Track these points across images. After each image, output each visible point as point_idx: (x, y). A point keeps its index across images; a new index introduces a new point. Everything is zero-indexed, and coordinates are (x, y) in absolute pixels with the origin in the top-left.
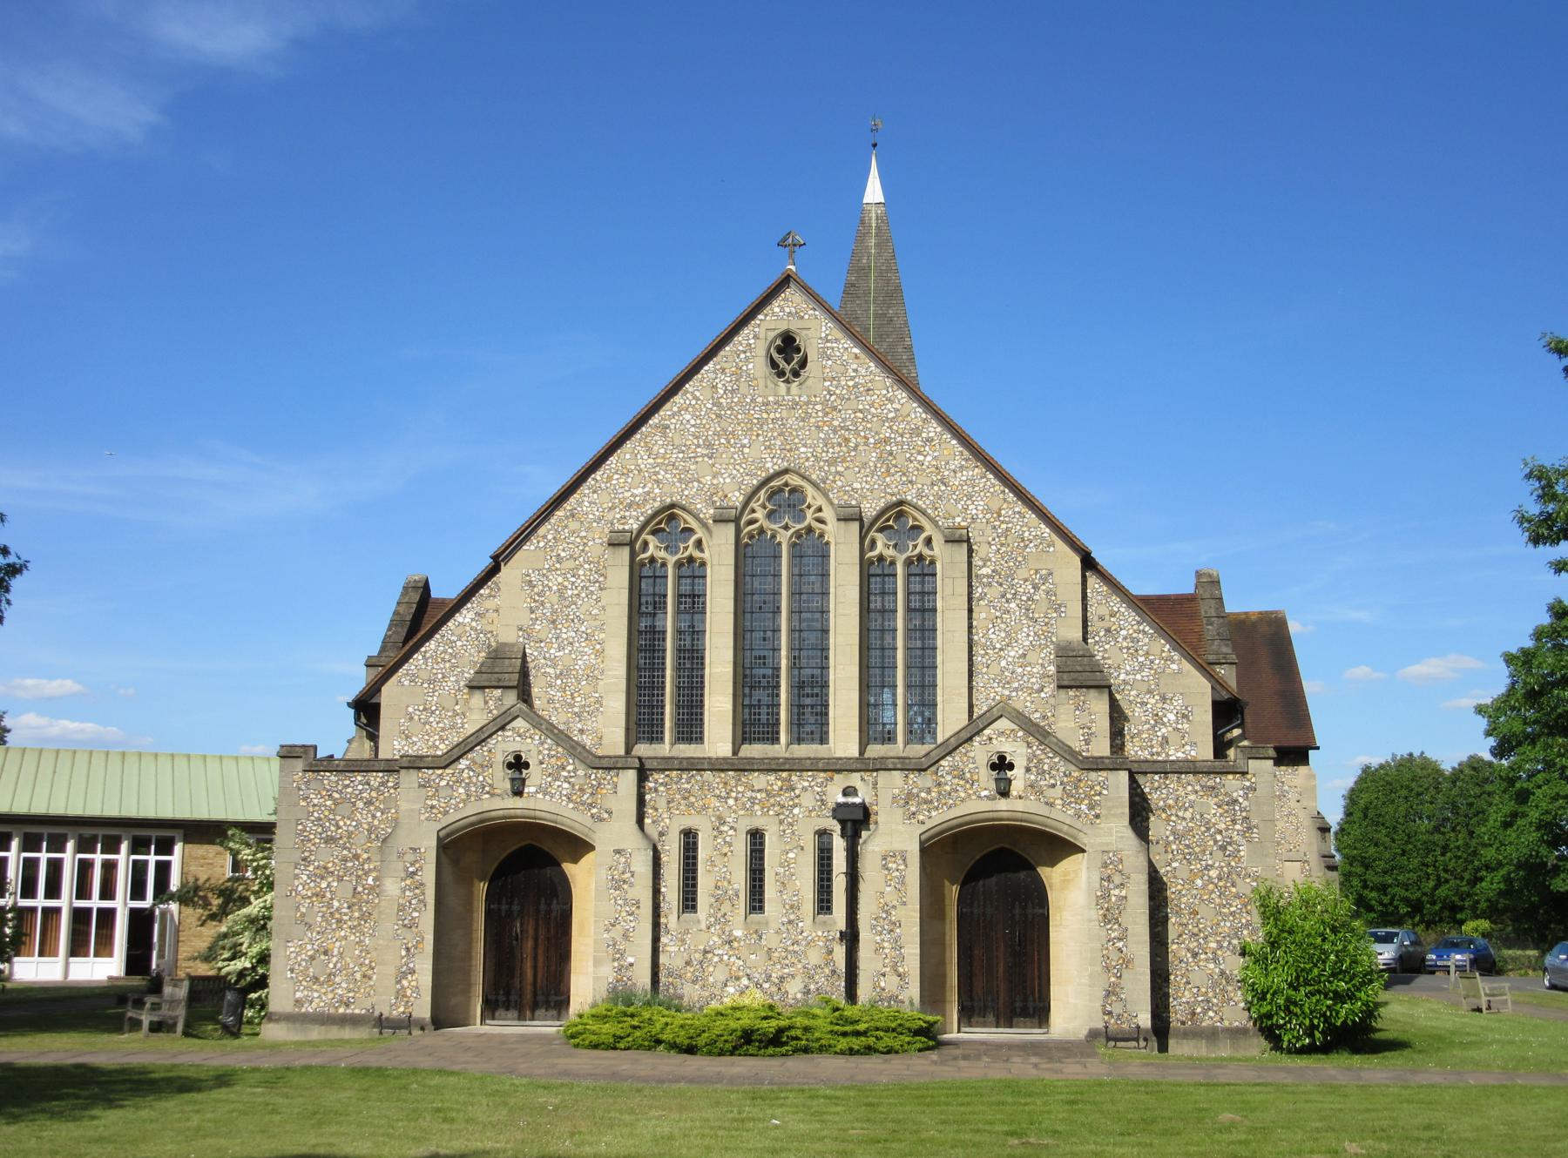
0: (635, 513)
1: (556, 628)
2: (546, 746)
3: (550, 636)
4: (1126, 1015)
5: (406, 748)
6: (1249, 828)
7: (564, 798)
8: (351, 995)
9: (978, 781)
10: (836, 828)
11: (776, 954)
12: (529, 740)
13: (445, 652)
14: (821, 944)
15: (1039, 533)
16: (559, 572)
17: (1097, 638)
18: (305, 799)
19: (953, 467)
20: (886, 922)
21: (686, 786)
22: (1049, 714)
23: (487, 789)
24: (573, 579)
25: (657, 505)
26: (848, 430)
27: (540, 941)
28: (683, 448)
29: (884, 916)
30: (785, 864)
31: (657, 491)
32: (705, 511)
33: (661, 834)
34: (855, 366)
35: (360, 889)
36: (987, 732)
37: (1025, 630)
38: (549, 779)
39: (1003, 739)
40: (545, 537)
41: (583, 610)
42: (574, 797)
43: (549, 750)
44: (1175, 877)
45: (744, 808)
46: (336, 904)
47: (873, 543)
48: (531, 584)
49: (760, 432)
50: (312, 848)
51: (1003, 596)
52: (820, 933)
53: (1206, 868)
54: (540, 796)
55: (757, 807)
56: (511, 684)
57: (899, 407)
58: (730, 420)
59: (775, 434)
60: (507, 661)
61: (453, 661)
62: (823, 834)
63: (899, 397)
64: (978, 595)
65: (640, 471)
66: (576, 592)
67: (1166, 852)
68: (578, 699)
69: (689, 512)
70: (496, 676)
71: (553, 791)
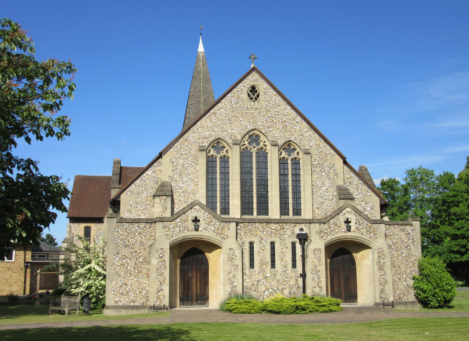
0: (206, 141)
1: (181, 177)
2: (206, 215)
3: (180, 179)
4: (386, 298)
5: (130, 216)
6: (414, 242)
7: (212, 232)
8: (135, 299)
9: (341, 227)
11: (280, 281)
12: (200, 213)
13: (142, 184)
14: (294, 278)
15: (331, 152)
16: (182, 159)
17: (347, 185)
18: (117, 232)
21: (250, 228)
22: (335, 207)
23: (186, 228)
24: (187, 161)
26: (273, 117)
27: (198, 279)
28: (222, 121)
29: (315, 269)
30: (282, 253)
31: (213, 134)
32: (229, 141)
33: (243, 243)
34: (275, 98)
35: (137, 263)
36: (343, 212)
37: (327, 181)
38: (207, 225)
39: (348, 214)
40: (177, 147)
41: (190, 171)
42: (216, 231)
44: (393, 256)
45: (269, 235)
46: (129, 268)
47: (281, 153)
49: (246, 117)
50: (120, 249)
51: (321, 171)
52: (294, 275)
53: (402, 254)
54: (204, 231)
55: (273, 235)
56: (169, 195)
57: (288, 111)
59: (251, 118)
60: (166, 187)
61: (145, 187)
62: (293, 244)
63: (288, 108)
64: (313, 170)
65: (208, 127)
66: (188, 165)
68: (189, 200)
70: (164, 192)
71: (209, 229)
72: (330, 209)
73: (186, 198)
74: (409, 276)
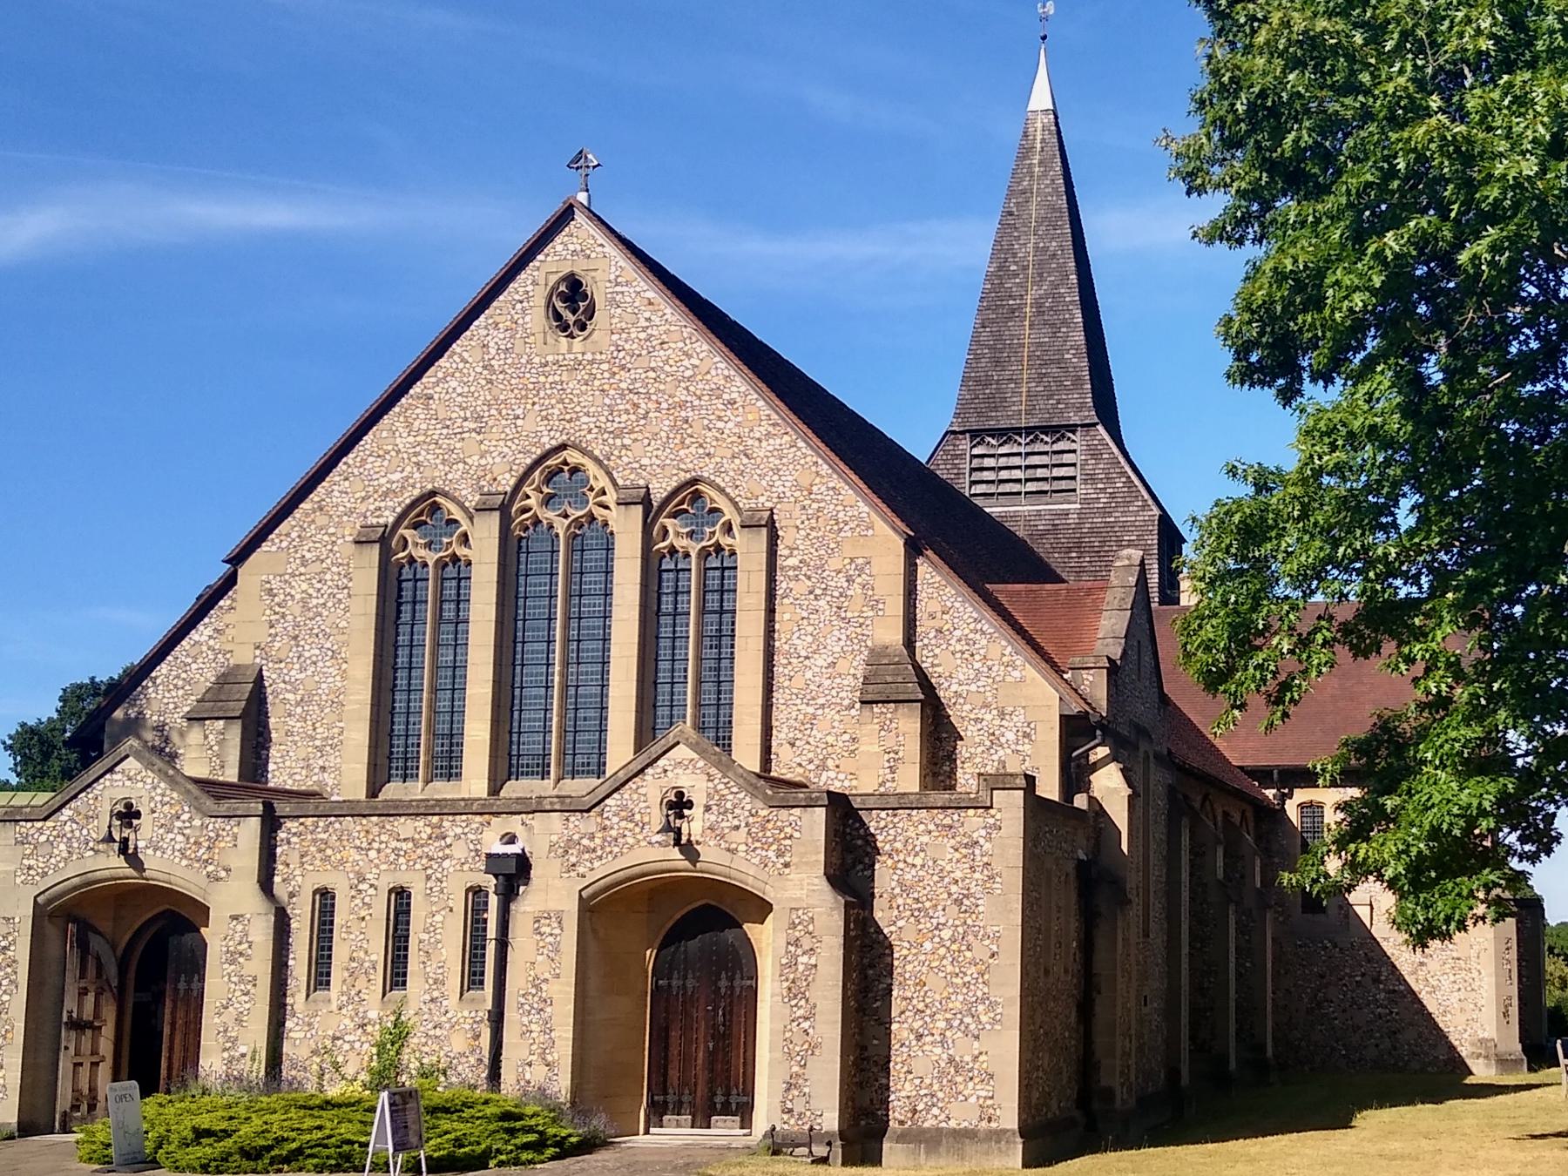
0: (391, 504)
1: (298, 646)
4: (808, 1113)
7: (177, 854)
9: (649, 823)
10: (490, 882)
13: (178, 677)
16: (303, 578)
19: (758, 435)
20: (536, 999)
24: (319, 586)
25: (417, 492)
29: (534, 991)
31: (417, 475)
33: (292, 895)
34: (647, 315)
36: (661, 762)
37: (836, 633)
38: (161, 831)
40: (288, 535)
43: (163, 795)
44: (900, 940)
48: (270, 592)
49: (536, 400)
52: (466, 1013)
55: (402, 860)
58: (501, 386)
59: (553, 401)
61: (187, 687)
62: (477, 892)
65: (398, 452)
66: (321, 601)
67: (891, 908)
69: (454, 500)
71: (165, 846)
72: (840, 744)
73: (309, 723)
74: (962, 1021)
